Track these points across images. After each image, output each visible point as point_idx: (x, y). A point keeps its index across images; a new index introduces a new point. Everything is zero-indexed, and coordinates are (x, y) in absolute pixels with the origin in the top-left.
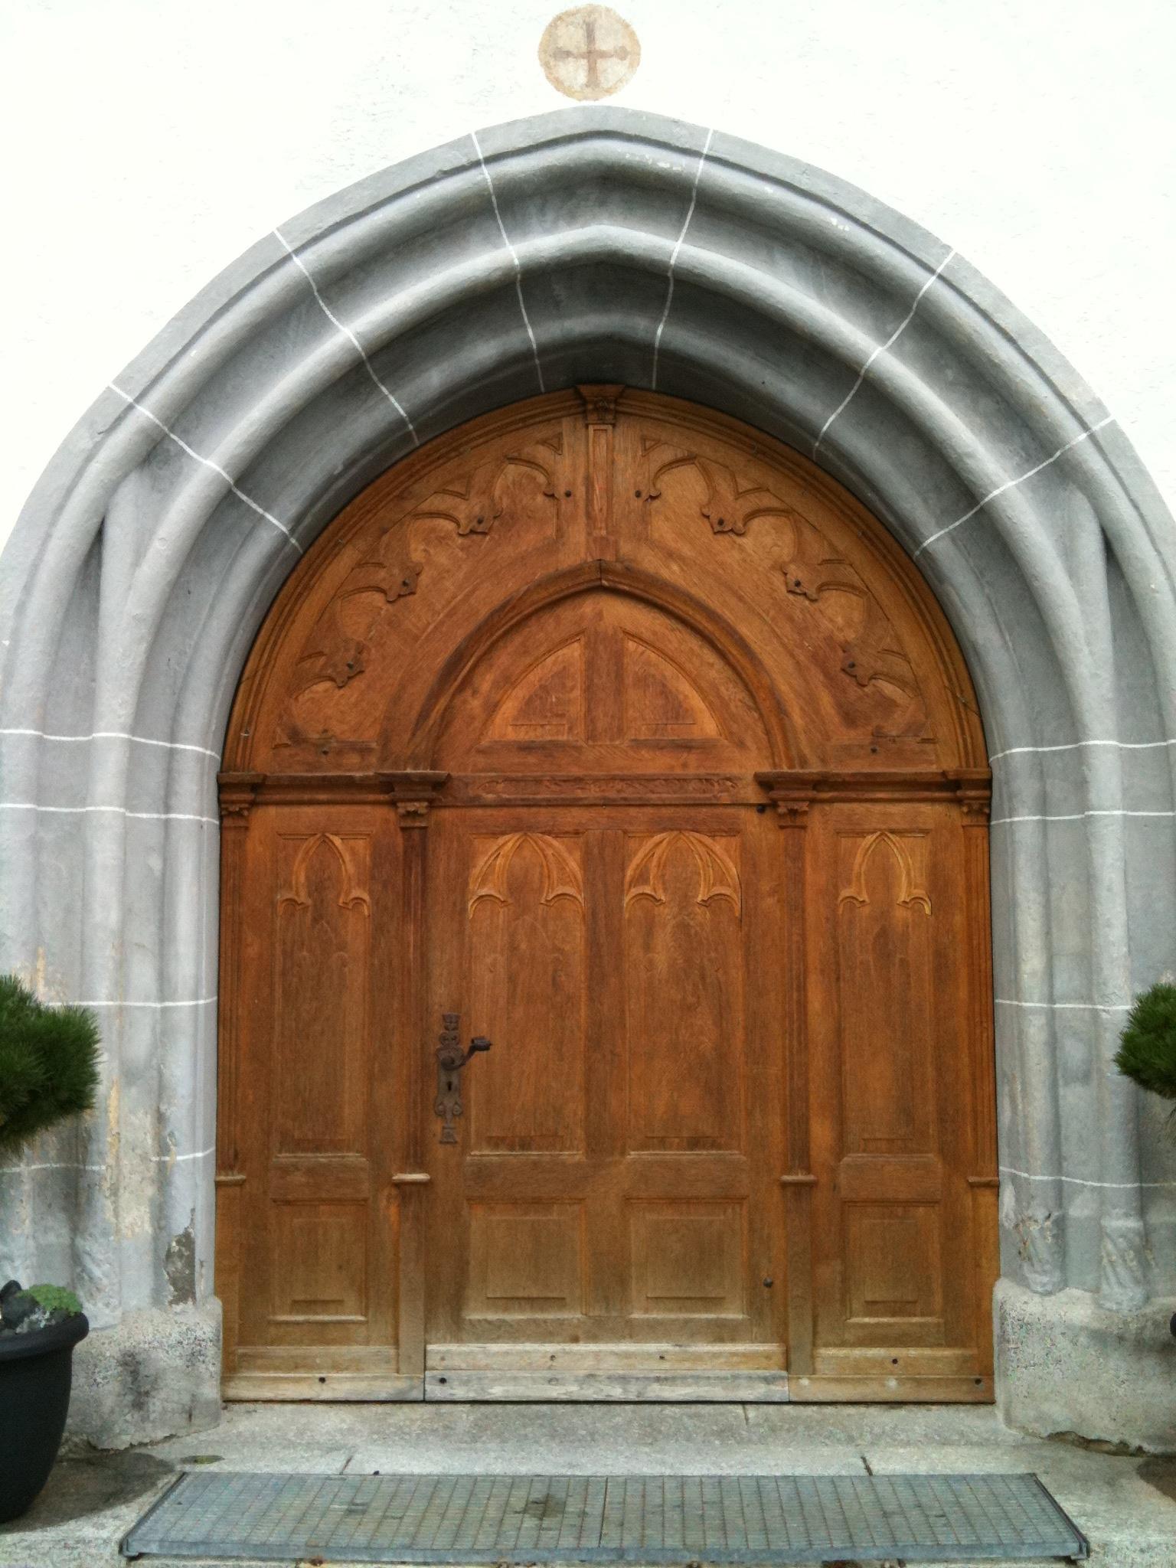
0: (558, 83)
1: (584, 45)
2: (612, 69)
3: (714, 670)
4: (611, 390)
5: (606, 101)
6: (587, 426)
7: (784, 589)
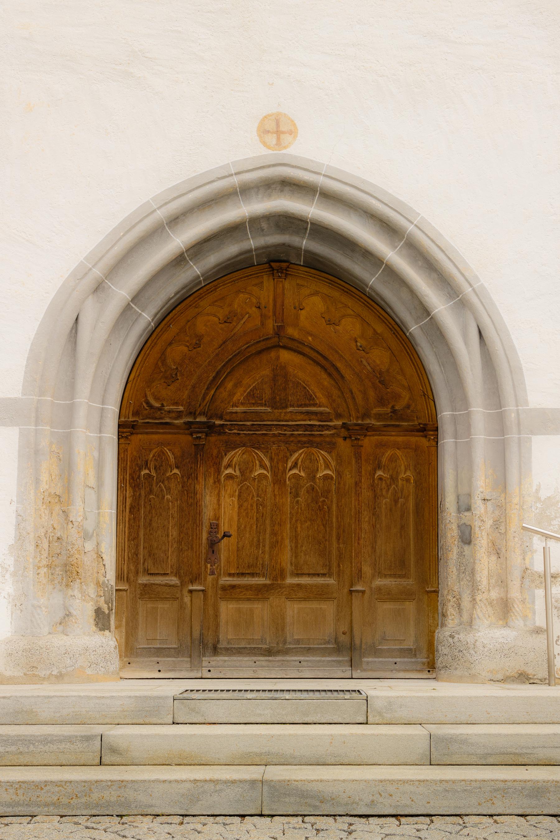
0: (265, 144)
1: (276, 128)
2: (286, 138)
3: (326, 381)
4: (284, 265)
5: (284, 151)
6: (274, 279)
7: (355, 348)
